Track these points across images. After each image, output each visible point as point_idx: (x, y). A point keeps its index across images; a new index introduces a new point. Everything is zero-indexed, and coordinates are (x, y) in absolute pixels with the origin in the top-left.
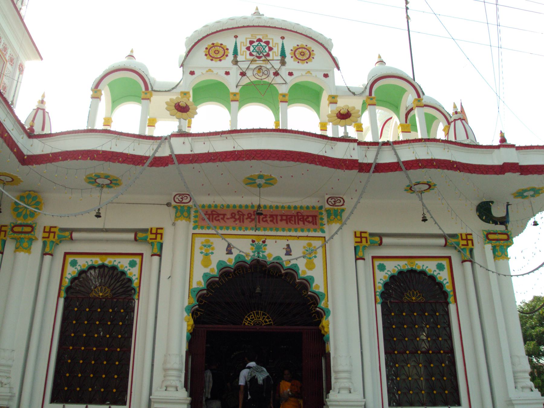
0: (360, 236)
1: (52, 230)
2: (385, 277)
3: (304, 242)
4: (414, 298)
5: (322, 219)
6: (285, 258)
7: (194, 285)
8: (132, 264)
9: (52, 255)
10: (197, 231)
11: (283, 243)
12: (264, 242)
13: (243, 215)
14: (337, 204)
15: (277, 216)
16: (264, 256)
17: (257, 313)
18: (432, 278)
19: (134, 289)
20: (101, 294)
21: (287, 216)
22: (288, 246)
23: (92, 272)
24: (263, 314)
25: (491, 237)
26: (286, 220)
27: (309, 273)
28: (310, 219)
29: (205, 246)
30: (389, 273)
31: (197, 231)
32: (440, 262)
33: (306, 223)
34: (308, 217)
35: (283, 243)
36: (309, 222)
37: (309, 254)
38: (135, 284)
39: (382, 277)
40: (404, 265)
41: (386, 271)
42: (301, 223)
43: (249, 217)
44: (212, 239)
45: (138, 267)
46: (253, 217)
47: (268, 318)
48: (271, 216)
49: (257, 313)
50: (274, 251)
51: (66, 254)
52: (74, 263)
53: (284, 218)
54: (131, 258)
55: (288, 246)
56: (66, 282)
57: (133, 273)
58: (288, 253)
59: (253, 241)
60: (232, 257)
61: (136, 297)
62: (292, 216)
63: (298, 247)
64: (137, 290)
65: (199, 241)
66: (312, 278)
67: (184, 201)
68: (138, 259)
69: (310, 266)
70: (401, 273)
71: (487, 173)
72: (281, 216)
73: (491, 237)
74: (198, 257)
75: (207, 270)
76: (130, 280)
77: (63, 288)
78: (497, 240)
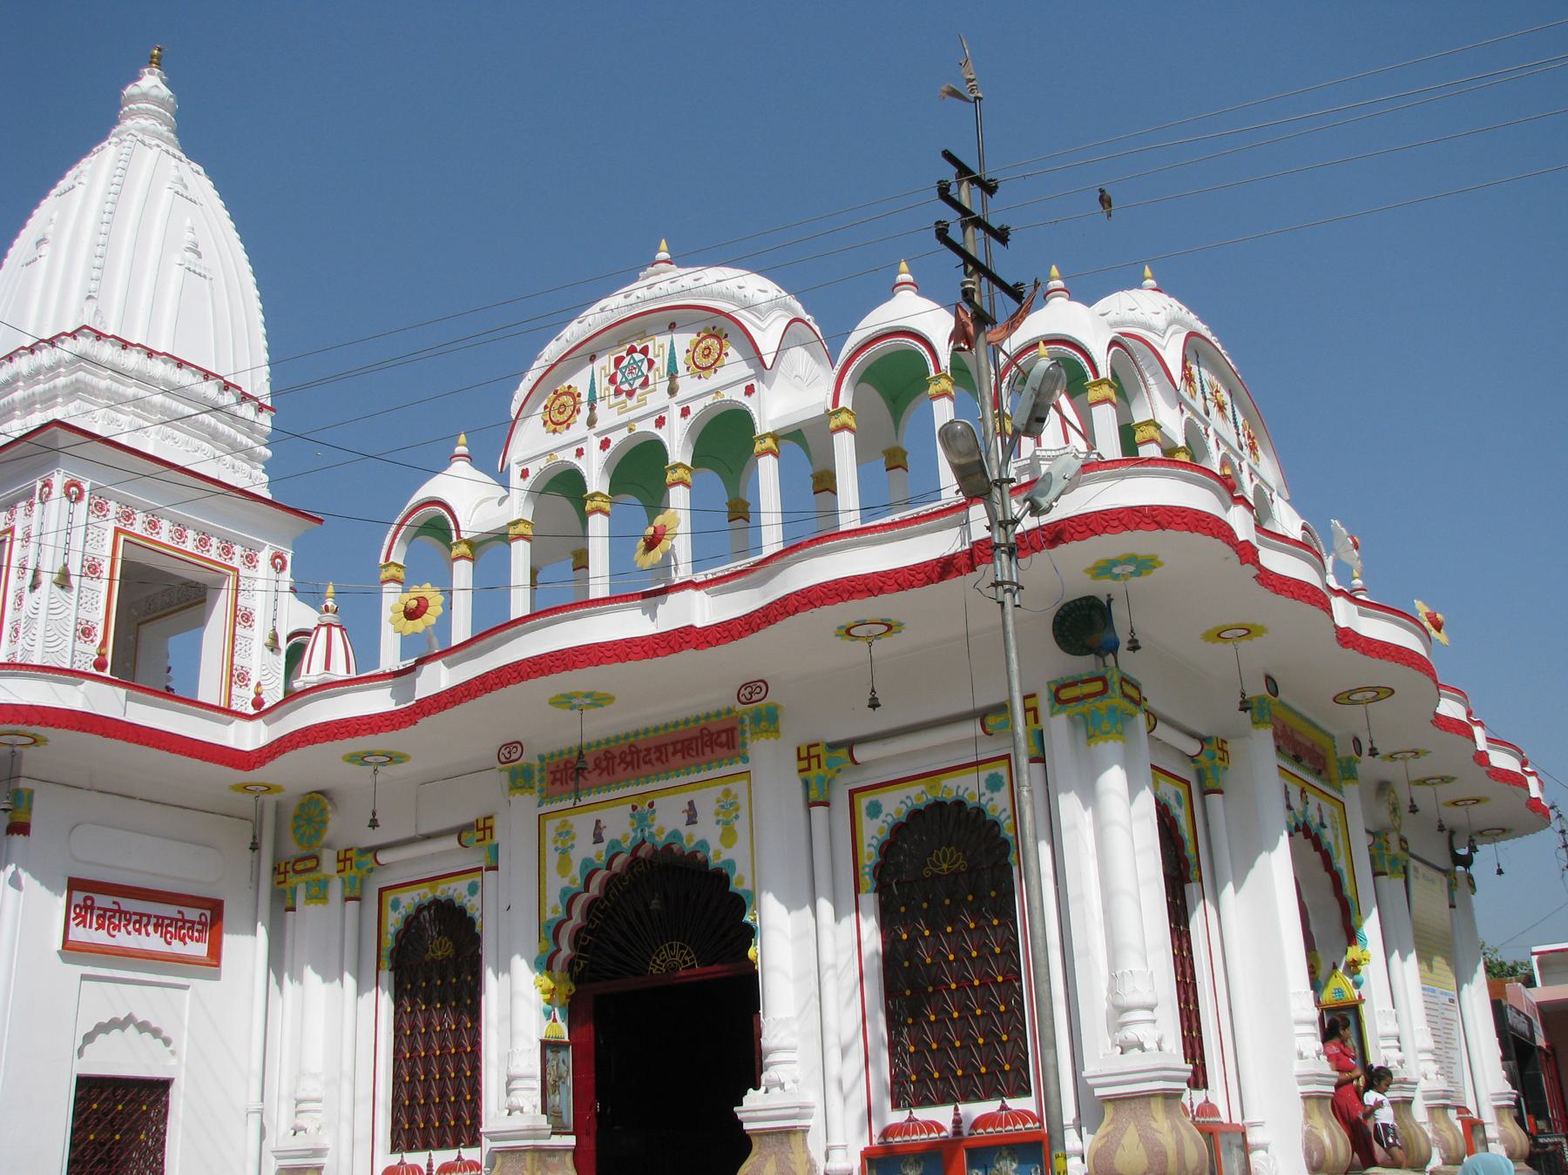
0: (807, 757)
1: (814, 751)
2: (881, 831)
3: (716, 791)
4: (945, 866)
5: (743, 732)
6: (685, 831)
7: (549, 915)
8: (994, 784)
9: (826, 804)
10: (546, 808)
11: (681, 801)
12: (651, 805)
13: (614, 757)
14: (755, 697)
15: (666, 745)
16: (651, 834)
17: (671, 947)
18: (898, 829)
19: (1005, 842)
20: (945, 866)
21: (682, 742)
22: (691, 803)
23: (426, 913)
24: (682, 948)
25: (1065, 694)
26: (682, 751)
27: (726, 854)
28: (723, 738)
29: (560, 834)
30: (890, 819)
31: (546, 808)
32: (993, 771)
33: (717, 749)
34: (719, 733)
35: (681, 801)
36: (721, 745)
37: (728, 811)
38: (1007, 832)
39: (873, 832)
40: (917, 795)
41: (882, 816)
42: (707, 750)
43: (622, 761)
44: (571, 819)
45: (1006, 788)
46: (629, 758)
47: (689, 954)
48: (658, 749)
49: (671, 947)
50: (668, 820)
51: (852, 793)
52: (874, 810)
53: (679, 746)
54: (985, 772)
55: (691, 803)
56: (389, 942)
57: (997, 805)
58: (692, 820)
59: (634, 808)
60: (603, 846)
61: (1012, 858)
62: (691, 739)
63: (707, 801)
64: (1012, 843)
65: (552, 826)
66: (731, 863)
67: (514, 757)
68: (1002, 769)
69: (728, 836)
70: (915, 814)
71: (599, 662)
72: (674, 744)
73: (1065, 694)
74: (552, 859)
75: (565, 882)
76: (995, 824)
77: (385, 953)
78: (1077, 699)
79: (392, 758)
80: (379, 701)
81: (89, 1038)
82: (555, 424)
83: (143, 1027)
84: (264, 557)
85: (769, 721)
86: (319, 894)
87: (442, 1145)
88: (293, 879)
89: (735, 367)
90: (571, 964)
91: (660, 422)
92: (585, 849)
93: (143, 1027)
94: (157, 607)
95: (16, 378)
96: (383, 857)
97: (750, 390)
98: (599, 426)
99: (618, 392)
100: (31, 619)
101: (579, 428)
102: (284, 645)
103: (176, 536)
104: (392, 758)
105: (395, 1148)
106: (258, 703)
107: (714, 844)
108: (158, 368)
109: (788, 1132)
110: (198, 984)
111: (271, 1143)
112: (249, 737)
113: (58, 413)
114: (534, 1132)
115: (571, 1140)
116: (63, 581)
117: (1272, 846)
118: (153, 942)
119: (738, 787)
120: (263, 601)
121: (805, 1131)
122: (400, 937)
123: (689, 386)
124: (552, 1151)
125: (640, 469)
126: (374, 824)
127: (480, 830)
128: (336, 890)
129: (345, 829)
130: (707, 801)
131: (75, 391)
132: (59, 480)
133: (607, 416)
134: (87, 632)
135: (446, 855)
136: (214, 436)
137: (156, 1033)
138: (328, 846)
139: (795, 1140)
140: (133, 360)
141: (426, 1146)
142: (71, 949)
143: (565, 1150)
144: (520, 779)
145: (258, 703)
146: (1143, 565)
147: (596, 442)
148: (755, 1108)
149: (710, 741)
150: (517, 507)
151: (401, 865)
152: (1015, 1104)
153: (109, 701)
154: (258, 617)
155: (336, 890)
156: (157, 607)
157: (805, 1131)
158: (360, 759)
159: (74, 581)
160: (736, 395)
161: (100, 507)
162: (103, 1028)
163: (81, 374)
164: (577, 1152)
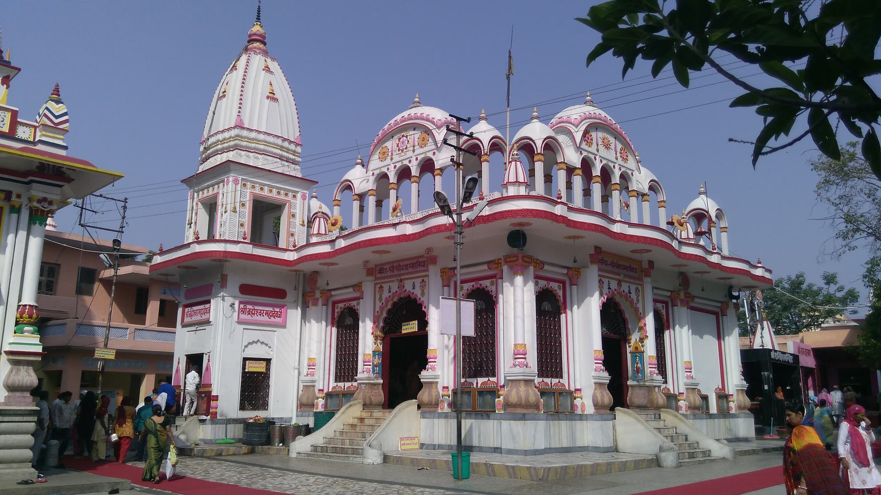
0: (443, 271)
11: (411, 281)
25: (508, 260)
69: (423, 294)
73: (508, 260)
79: (332, 264)
80: (326, 249)
81: (246, 346)
82: (382, 159)
83: (262, 343)
84: (299, 195)
85: (433, 260)
86: (315, 304)
87: (348, 381)
88: (308, 298)
89: (431, 146)
90: (383, 328)
91: (410, 161)
92: (386, 294)
93: (262, 343)
94: (265, 216)
95: (218, 141)
96: (333, 293)
97: (434, 153)
98: (394, 161)
99: (399, 150)
100: (225, 222)
101: (388, 161)
102: (306, 223)
103: (270, 192)
104: (332, 264)
105: (336, 381)
106: (294, 246)
107: (419, 296)
108: (262, 137)
109: (432, 383)
110: (280, 331)
111: (302, 378)
112: (291, 256)
113: (230, 156)
114: (369, 379)
115: (382, 381)
116: (234, 211)
117: (592, 295)
118: (265, 318)
119: (426, 279)
120: (299, 207)
121: (437, 383)
122: (340, 317)
123: (419, 150)
124: (375, 384)
125: (404, 173)
126: (328, 284)
127: (357, 287)
128: (320, 302)
129: (321, 283)
130: (418, 282)
131: (236, 148)
132: (231, 179)
133: (396, 158)
134: (242, 225)
135: (349, 293)
136: (281, 158)
137: (266, 345)
138: (318, 289)
139: (434, 385)
140: (253, 135)
141: (344, 381)
142: (239, 322)
143: (379, 384)
144: (370, 272)
145: (294, 246)
146: (528, 224)
147: (393, 166)
148: (425, 375)
149: (420, 263)
150: (370, 185)
151: (339, 295)
152: (492, 379)
153: (249, 249)
154: (297, 216)
155: (320, 302)
156: (265, 216)
157: (437, 383)
158: (325, 264)
159: (238, 209)
160: (430, 155)
161: (245, 185)
162: (249, 343)
163: (237, 142)
164: (383, 384)
